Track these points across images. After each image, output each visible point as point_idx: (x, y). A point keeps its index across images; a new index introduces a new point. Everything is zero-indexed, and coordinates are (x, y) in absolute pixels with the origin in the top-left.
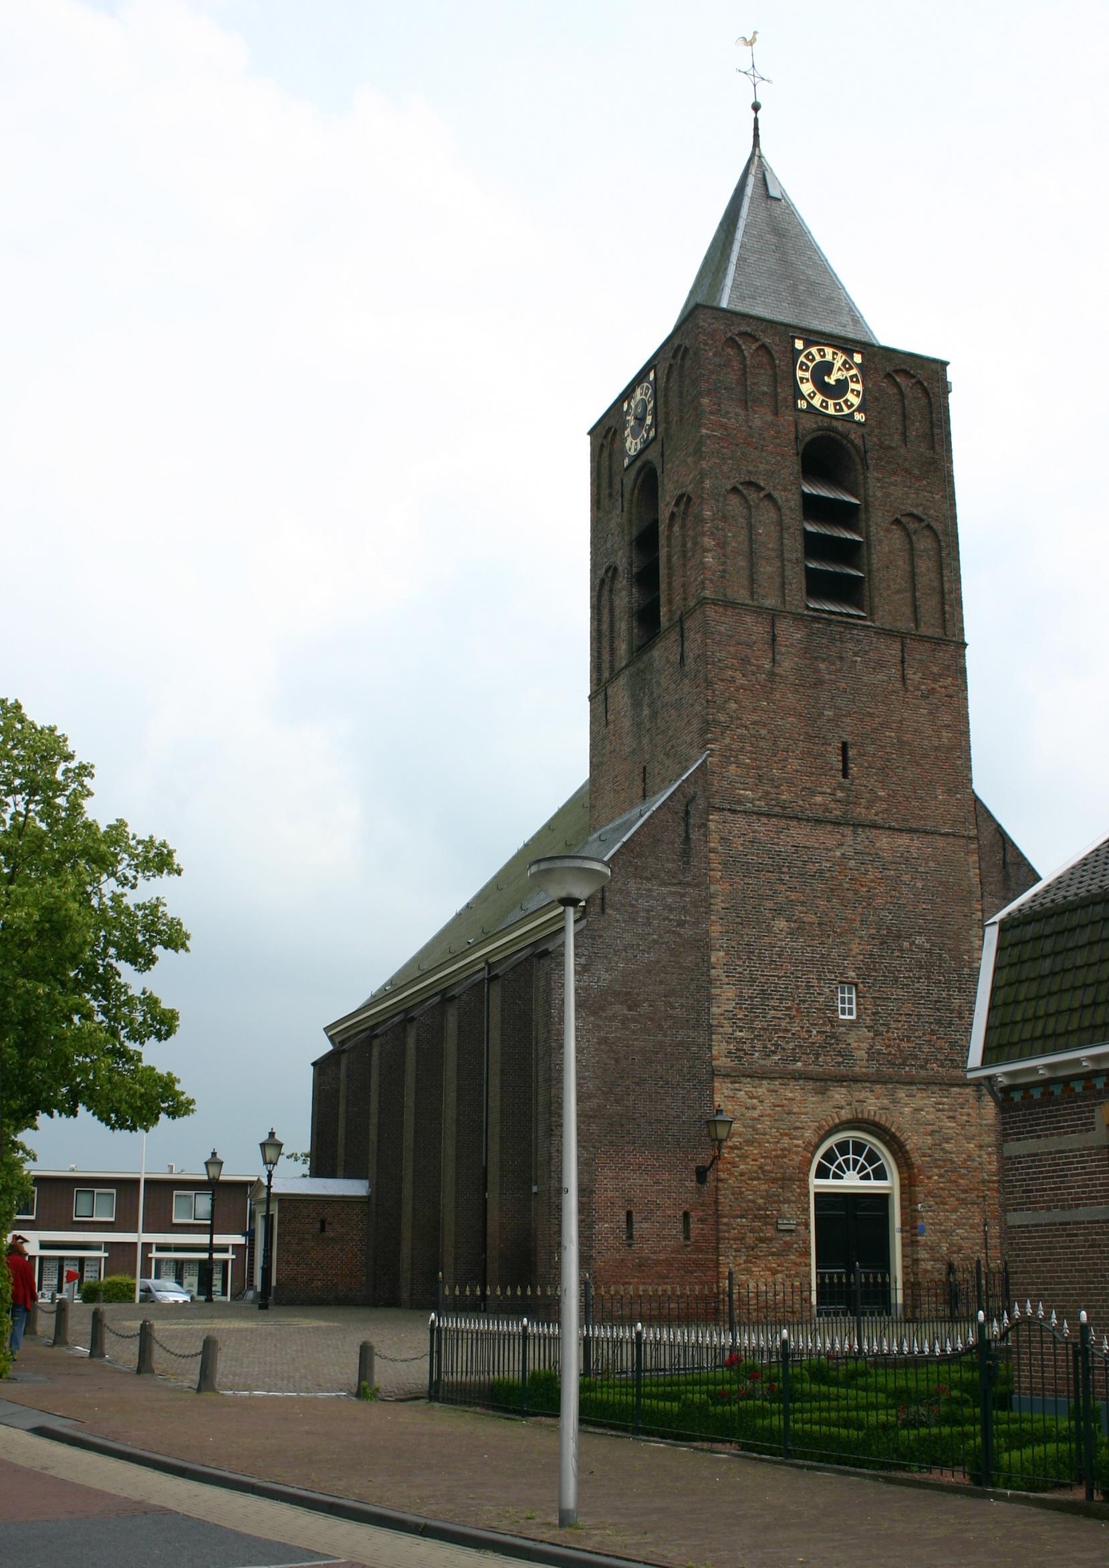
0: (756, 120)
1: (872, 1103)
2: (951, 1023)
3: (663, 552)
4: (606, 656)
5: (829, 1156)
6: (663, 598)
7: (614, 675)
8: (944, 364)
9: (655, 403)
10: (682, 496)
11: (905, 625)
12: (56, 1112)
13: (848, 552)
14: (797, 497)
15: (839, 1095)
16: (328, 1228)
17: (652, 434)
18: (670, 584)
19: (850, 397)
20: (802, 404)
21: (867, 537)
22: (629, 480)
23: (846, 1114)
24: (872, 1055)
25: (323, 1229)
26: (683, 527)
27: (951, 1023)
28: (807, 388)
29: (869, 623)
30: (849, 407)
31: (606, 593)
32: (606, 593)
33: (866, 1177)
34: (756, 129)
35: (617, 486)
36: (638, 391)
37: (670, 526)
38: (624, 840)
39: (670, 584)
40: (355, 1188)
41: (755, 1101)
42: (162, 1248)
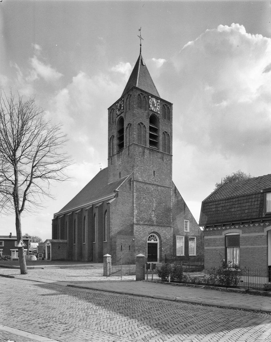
0: (141, 48)
1: (156, 229)
2: (167, 217)
3: (125, 134)
4: (111, 151)
5: (150, 237)
7: (113, 155)
8: (171, 104)
10: (129, 124)
13: (155, 137)
14: (149, 126)
15: (151, 228)
18: (126, 140)
21: (159, 135)
23: (152, 231)
24: (157, 222)
27: (167, 217)
32: (111, 140)
33: (155, 241)
34: (141, 50)
38: (121, 185)
39: (126, 140)
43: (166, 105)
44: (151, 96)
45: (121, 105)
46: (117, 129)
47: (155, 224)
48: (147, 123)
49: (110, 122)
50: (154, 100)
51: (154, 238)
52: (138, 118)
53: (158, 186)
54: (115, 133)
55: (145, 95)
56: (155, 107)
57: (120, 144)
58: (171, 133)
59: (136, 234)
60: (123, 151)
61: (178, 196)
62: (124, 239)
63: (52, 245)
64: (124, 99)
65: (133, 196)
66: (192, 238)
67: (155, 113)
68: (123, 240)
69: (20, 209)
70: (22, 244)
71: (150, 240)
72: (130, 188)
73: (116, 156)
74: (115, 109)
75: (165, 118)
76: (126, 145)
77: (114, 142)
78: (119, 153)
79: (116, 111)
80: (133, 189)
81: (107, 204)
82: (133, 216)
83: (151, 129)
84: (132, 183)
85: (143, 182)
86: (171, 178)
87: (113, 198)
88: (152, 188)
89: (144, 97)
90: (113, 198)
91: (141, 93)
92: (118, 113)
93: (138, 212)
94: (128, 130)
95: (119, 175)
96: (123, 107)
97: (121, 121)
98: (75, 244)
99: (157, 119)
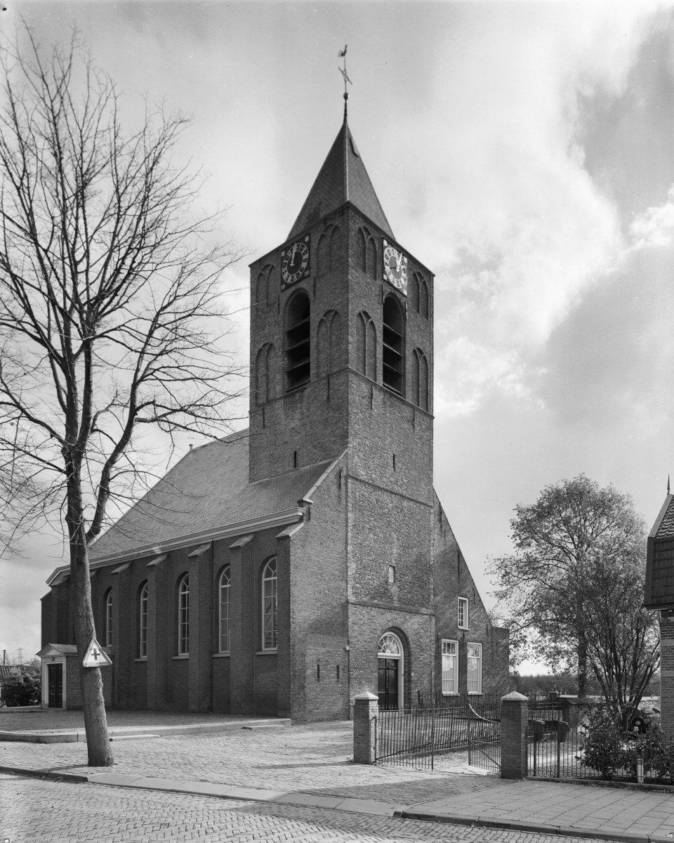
7: (269, 402)
8: (434, 275)
10: (329, 312)
15: (389, 616)
20: (385, 278)
21: (405, 354)
34: (346, 111)
43: (419, 274)
44: (388, 242)
45: (298, 256)
46: (284, 326)
47: (396, 604)
48: (377, 316)
53: (403, 497)
54: (278, 337)
55: (375, 234)
56: (398, 276)
57: (292, 370)
58: (432, 355)
59: (353, 631)
60: (305, 388)
61: (445, 531)
62: (324, 645)
63: (67, 661)
64: (309, 239)
65: (347, 520)
66: (449, 644)
67: (396, 292)
68: (323, 650)
69: (87, 528)
70: (95, 655)
71: (384, 652)
72: (339, 497)
73: (279, 405)
74: (278, 269)
75: (418, 312)
76: (318, 375)
77: (271, 362)
78: (293, 395)
80: (347, 502)
81: (279, 539)
82: (347, 580)
84: (343, 481)
85: (369, 484)
86: (430, 480)
87: (296, 523)
88: (389, 502)
89: (372, 239)
90: (296, 523)
91: (364, 228)
93: (357, 567)
95: (291, 459)
97: (301, 305)
99: (400, 310)
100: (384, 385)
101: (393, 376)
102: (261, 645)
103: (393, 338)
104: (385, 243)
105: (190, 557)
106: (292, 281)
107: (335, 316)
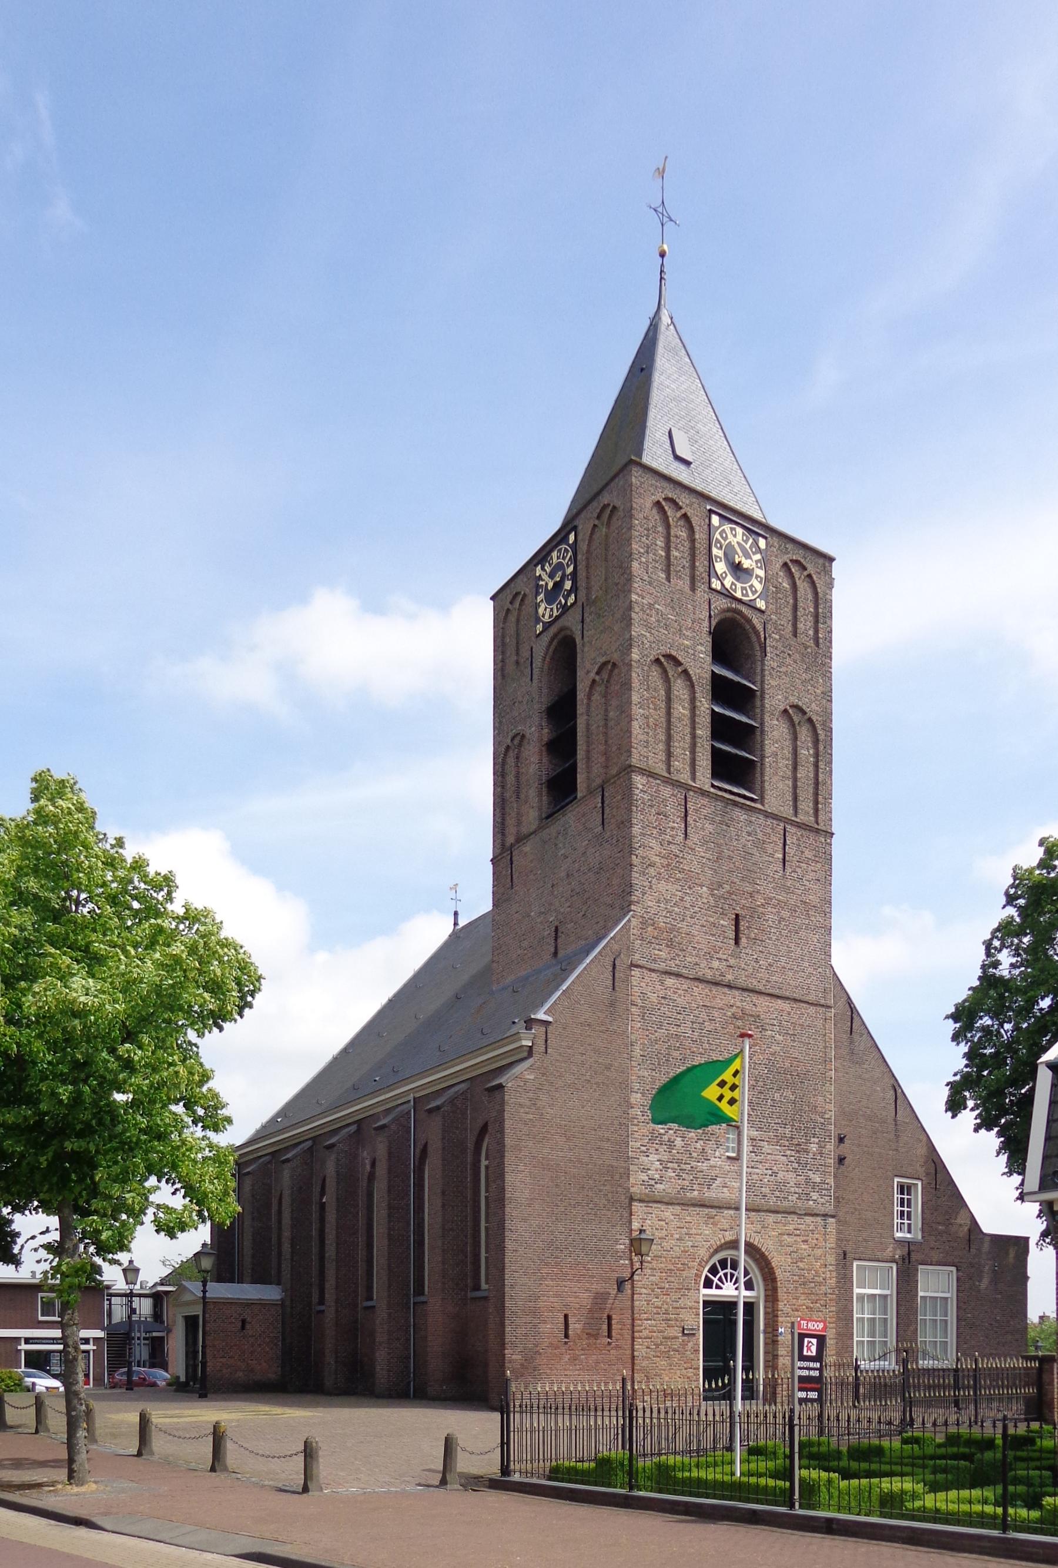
0: (662, 265)
3: (581, 722)
6: (581, 766)
7: (520, 839)
8: (831, 560)
9: (575, 568)
10: (605, 664)
11: (787, 811)
12: (978, 1121)
16: (248, 1326)
17: (572, 599)
19: (755, 582)
20: (716, 584)
21: (762, 724)
22: (540, 648)
25: (243, 1328)
26: (605, 696)
28: (720, 567)
29: (759, 806)
30: (754, 592)
31: (511, 761)
32: (511, 761)
35: (526, 654)
36: (555, 554)
37: (589, 696)
40: (271, 1293)
41: (663, 1223)
42: (28, 1341)
48: (701, 662)
49: (503, 824)
50: (736, 536)
51: (729, 1271)
52: (665, 624)
67: (744, 609)
71: (718, 1287)
74: (530, 597)
79: (537, 606)
83: (721, 690)
92: (547, 616)
94: (596, 697)
96: (574, 574)
98: (322, 1308)
100: (713, 786)
101: (735, 762)
102: (479, 1279)
103: (733, 695)
104: (715, 520)
105: (376, 1129)
106: (550, 616)
107: (613, 670)
